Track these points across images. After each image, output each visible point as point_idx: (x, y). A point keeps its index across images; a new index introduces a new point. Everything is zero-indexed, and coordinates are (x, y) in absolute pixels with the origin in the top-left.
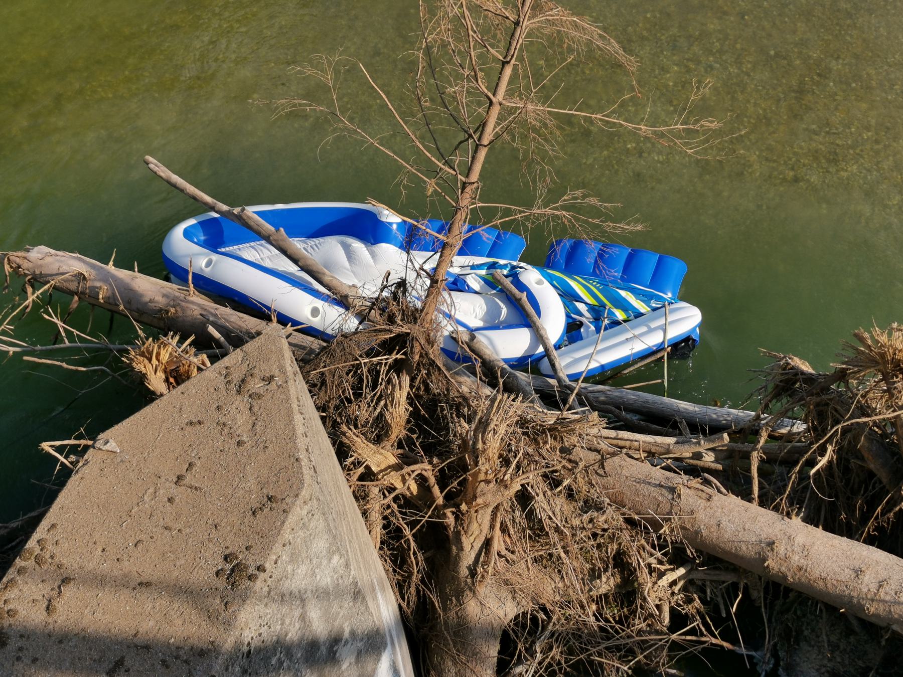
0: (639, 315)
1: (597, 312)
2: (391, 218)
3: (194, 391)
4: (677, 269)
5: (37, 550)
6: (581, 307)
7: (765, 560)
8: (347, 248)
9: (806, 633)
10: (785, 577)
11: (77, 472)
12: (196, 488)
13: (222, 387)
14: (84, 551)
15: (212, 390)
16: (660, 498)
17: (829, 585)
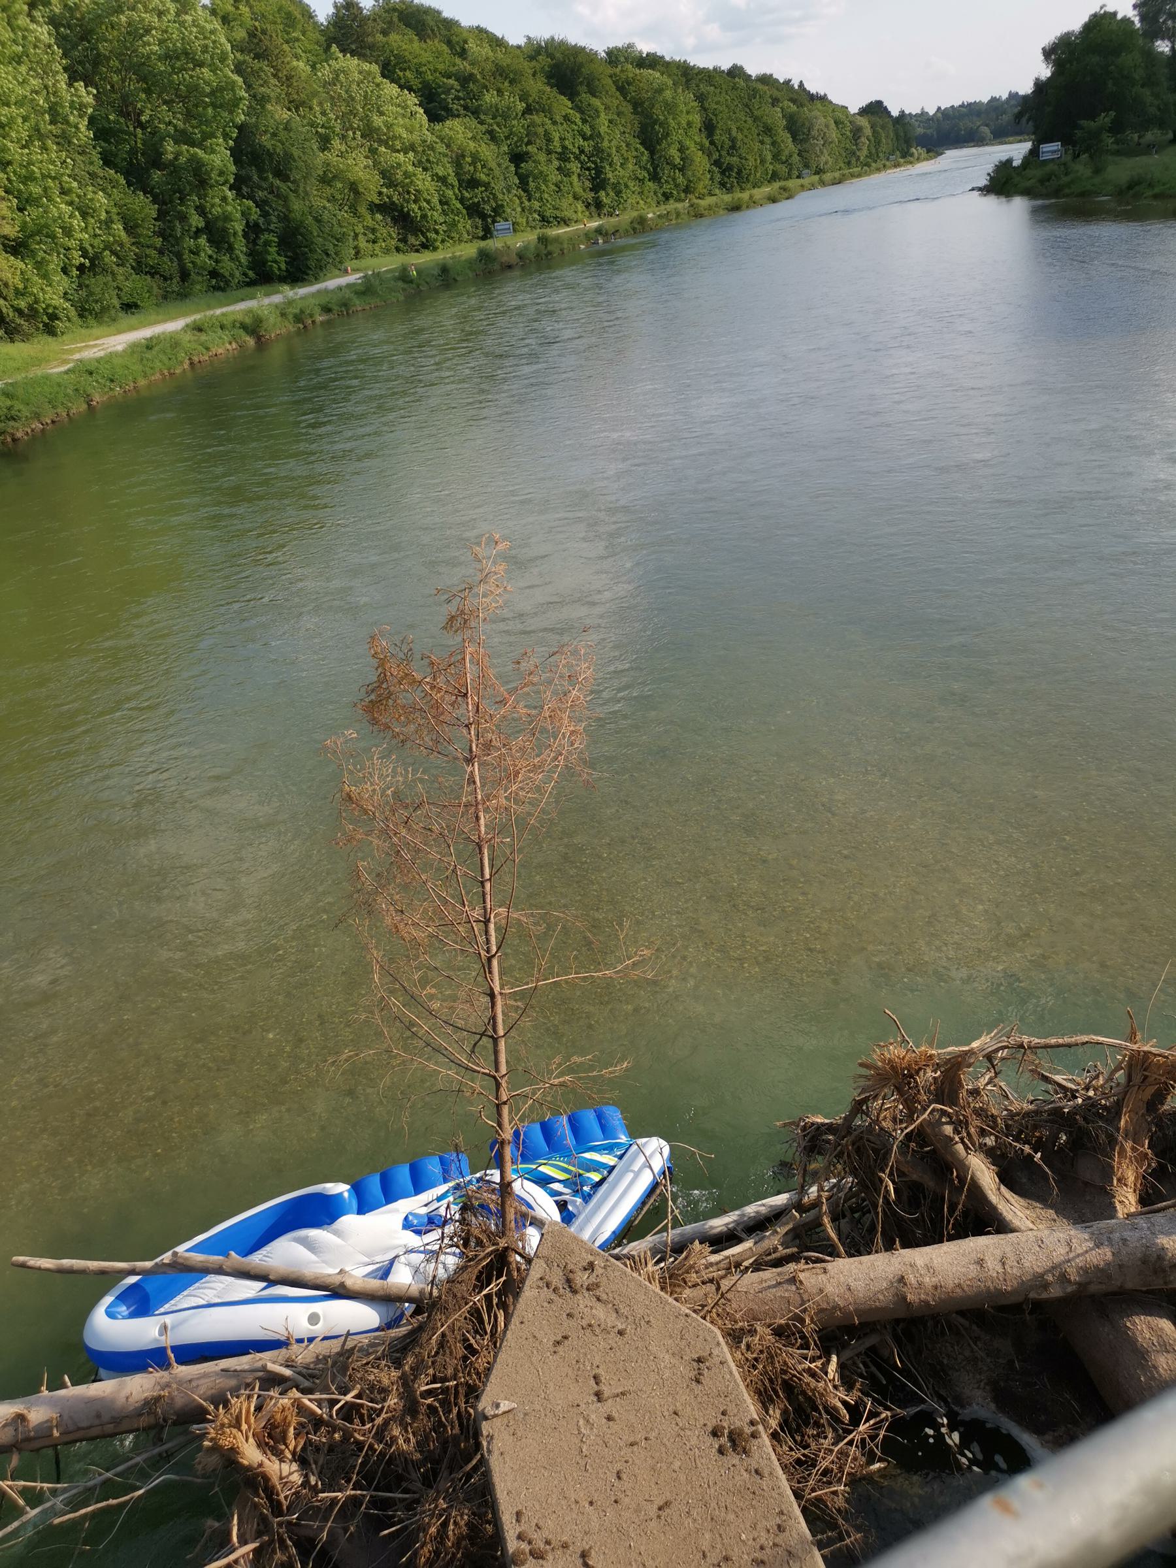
0: (612, 1169)
1: (575, 1184)
2: (340, 1188)
3: (530, 1316)
4: (615, 1116)
5: (524, 1546)
6: (556, 1186)
7: (905, 1298)
8: (305, 1242)
9: (945, 1362)
10: (927, 1303)
11: (489, 1451)
12: (623, 1394)
13: (553, 1296)
14: (574, 1516)
15: (546, 1304)
16: (787, 1295)
17: (966, 1288)
